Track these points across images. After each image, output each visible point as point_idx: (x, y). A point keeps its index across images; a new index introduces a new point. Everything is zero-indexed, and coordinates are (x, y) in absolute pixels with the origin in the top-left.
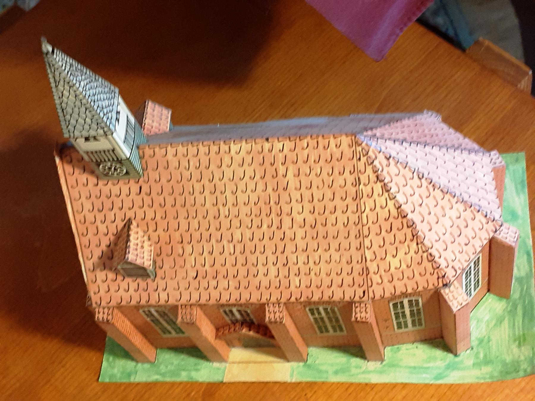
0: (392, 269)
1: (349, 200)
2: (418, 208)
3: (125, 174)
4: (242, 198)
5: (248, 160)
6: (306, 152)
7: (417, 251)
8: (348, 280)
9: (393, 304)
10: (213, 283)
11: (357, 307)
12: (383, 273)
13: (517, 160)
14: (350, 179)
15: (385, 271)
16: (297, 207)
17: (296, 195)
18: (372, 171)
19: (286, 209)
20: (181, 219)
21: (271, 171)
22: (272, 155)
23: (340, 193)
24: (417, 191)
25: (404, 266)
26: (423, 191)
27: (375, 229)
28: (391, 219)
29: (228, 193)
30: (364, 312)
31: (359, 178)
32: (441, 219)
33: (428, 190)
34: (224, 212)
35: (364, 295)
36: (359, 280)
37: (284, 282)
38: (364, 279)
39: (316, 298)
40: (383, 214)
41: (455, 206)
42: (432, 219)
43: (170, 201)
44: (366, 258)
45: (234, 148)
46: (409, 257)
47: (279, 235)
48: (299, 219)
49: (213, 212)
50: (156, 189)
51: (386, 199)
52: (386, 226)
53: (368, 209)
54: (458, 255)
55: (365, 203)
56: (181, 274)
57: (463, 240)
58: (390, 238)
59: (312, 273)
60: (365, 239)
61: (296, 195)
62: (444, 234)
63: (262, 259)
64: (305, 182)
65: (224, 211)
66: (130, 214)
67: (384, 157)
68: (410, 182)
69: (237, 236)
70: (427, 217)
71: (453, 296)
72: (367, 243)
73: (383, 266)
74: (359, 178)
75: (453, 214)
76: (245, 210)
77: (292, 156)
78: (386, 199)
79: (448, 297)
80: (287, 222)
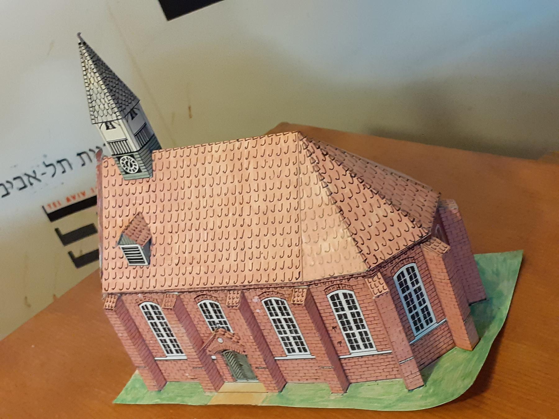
1: (292, 187)
2: (347, 200)
3: (138, 172)
4: (217, 190)
5: (223, 158)
7: (320, 205)
8: (288, 263)
9: (331, 297)
10: (189, 269)
11: (296, 292)
12: (316, 255)
13: (516, 256)
14: (293, 169)
15: (317, 253)
16: (254, 195)
17: (254, 186)
18: (309, 162)
20: (174, 213)
21: (238, 166)
22: (239, 151)
23: (286, 182)
24: (349, 186)
25: (332, 250)
26: (354, 187)
27: (310, 213)
28: (323, 206)
29: (207, 186)
30: (301, 296)
31: (299, 168)
37: (241, 267)
38: (299, 260)
40: (317, 201)
41: (383, 206)
42: (360, 212)
43: (168, 197)
44: (302, 240)
45: (215, 147)
46: (336, 241)
48: (255, 206)
50: (160, 187)
51: (320, 187)
52: (319, 212)
53: (305, 196)
54: (381, 248)
55: (303, 190)
57: (387, 236)
58: (322, 223)
61: (254, 186)
63: (226, 243)
65: (203, 203)
67: (321, 153)
68: (342, 178)
69: (210, 226)
70: (354, 209)
72: (303, 227)
74: (299, 168)
75: (381, 213)
76: (218, 200)
77: (253, 152)
78: (320, 187)
79: (371, 285)
80: (246, 211)
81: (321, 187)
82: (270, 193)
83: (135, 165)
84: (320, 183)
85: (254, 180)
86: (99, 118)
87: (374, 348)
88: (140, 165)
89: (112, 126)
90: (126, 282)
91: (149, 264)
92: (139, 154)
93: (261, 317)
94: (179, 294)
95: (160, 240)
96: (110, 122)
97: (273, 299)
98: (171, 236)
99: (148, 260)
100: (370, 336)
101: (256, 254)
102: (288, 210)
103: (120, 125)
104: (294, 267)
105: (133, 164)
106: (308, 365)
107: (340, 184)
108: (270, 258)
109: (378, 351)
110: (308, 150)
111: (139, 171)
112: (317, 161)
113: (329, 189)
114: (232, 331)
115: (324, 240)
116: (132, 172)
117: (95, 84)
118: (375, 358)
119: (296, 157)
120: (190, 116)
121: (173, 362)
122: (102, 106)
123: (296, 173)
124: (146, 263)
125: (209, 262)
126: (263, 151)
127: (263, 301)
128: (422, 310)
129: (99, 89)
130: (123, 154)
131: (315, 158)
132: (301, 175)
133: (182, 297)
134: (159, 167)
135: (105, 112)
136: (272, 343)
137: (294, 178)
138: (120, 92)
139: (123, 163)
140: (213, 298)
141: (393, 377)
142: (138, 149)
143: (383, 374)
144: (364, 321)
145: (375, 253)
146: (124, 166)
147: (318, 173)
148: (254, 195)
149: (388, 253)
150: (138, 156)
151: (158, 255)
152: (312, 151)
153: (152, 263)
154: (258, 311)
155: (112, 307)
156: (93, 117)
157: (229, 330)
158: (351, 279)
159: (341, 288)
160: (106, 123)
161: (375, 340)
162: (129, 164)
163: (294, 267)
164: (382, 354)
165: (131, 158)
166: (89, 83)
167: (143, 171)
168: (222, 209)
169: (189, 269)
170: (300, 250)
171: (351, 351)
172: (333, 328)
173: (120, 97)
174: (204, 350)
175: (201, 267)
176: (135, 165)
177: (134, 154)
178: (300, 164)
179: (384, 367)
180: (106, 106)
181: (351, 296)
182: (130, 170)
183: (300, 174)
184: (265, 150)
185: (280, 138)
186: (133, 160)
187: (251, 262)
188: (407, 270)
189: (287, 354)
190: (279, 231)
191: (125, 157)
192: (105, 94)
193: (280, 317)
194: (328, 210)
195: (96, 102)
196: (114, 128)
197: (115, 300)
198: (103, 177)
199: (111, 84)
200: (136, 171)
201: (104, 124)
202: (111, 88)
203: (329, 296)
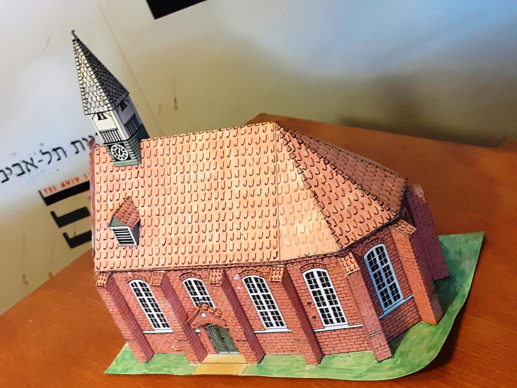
0: (299, 234)
2: (321, 185)
5: (206, 146)
6: (244, 136)
10: (175, 249)
12: (292, 236)
14: (271, 156)
15: (293, 235)
16: (235, 181)
19: (228, 184)
23: (264, 169)
24: (322, 173)
25: (307, 231)
27: (287, 197)
28: (299, 191)
31: (277, 155)
32: (341, 198)
33: (332, 174)
34: (188, 189)
35: (277, 256)
36: (274, 242)
37: (223, 248)
39: (260, 341)
40: (294, 186)
41: (354, 191)
45: (199, 136)
47: (222, 205)
48: (236, 191)
49: (181, 189)
50: (148, 173)
51: (296, 173)
52: (295, 196)
53: (282, 181)
55: (280, 176)
56: (155, 242)
57: (358, 218)
58: (297, 207)
59: (242, 237)
60: (279, 206)
62: (342, 210)
63: (209, 225)
64: (242, 159)
65: (188, 188)
66: (129, 194)
68: (316, 165)
70: (328, 194)
71: (347, 263)
72: (281, 210)
73: (292, 230)
74: (277, 155)
75: (352, 197)
77: (234, 141)
78: (296, 173)
80: (228, 196)
81: (297, 173)
82: (250, 179)
83: (125, 153)
84: (296, 169)
85: (235, 166)
86: (92, 109)
87: (346, 323)
88: (130, 153)
89: (104, 116)
90: (117, 261)
91: (138, 244)
92: (128, 143)
93: (242, 294)
94: (166, 272)
95: (148, 222)
96: (102, 113)
97: (252, 277)
98: (159, 219)
99: (137, 241)
100: (342, 311)
101: (237, 235)
102: (267, 194)
103: (111, 116)
104: (272, 247)
105: (123, 152)
106: (285, 338)
107: (315, 170)
108: (250, 239)
109: (350, 325)
110: (285, 139)
111: (129, 158)
112: (293, 149)
113: (304, 175)
114: (214, 307)
115: (299, 222)
116: (122, 159)
117: (88, 78)
118: (347, 331)
119: (274, 145)
120: (176, 108)
121: (160, 336)
122: (94, 98)
123: (274, 161)
124: (135, 244)
125: (193, 243)
126: (244, 140)
127: (243, 279)
128: (391, 287)
129: (92, 83)
130: (113, 142)
131: (291, 146)
132: (279, 162)
133: (168, 275)
134: (147, 155)
135: (97, 103)
136: (251, 318)
137: (271, 165)
138: (111, 85)
139: (114, 151)
140: (197, 276)
141: (364, 349)
142: (128, 138)
143: (354, 346)
144: (337, 297)
145: (347, 234)
146: (115, 154)
147: (294, 160)
148: (235, 181)
149: (359, 235)
150: (128, 144)
151: (146, 236)
152: (289, 140)
153: (140, 243)
154: (238, 288)
155: (103, 284)
156: (86, 109)
157: (212, 306)
158: (325, 258)
159: (316, 267)
160: (98, 114)
161: (347, 315)
162: (119, 152)
163: (272, 247)
164: (353, 328)
165: (122, 146)
166: (82, 77)
167: (132, 158)
168: (205, 194)
169: (175, 249)
170: (277, 232)
171: (325, 325)
172: (308, 303)
173: (111, 90)
174: (189, 324)
175: (186, 248)
176: (125, 153)
177: (124, 142)
178: (278, 152)
179: (355, 340)
180: (98, 98)
181: (325, 274)
182: (120, 158)
183: (277, 161)
184: (245, 139)
185: (259, 128)
186: (123, 148)
187: (232, 242)
188: (377, 250)
189: (266, 328)
190: (258, 214)
191: (116, 145)
192: (97, 87)
193: (259, 293)
194: (303, 194)
195: (89, 94)
196: (105, 118)
197: (107, 278)
198: (95, 164)
199: (103, 78)
200: (126, 158)
201: (96, 115)
202: (103, 82)
203: (304, 274)
